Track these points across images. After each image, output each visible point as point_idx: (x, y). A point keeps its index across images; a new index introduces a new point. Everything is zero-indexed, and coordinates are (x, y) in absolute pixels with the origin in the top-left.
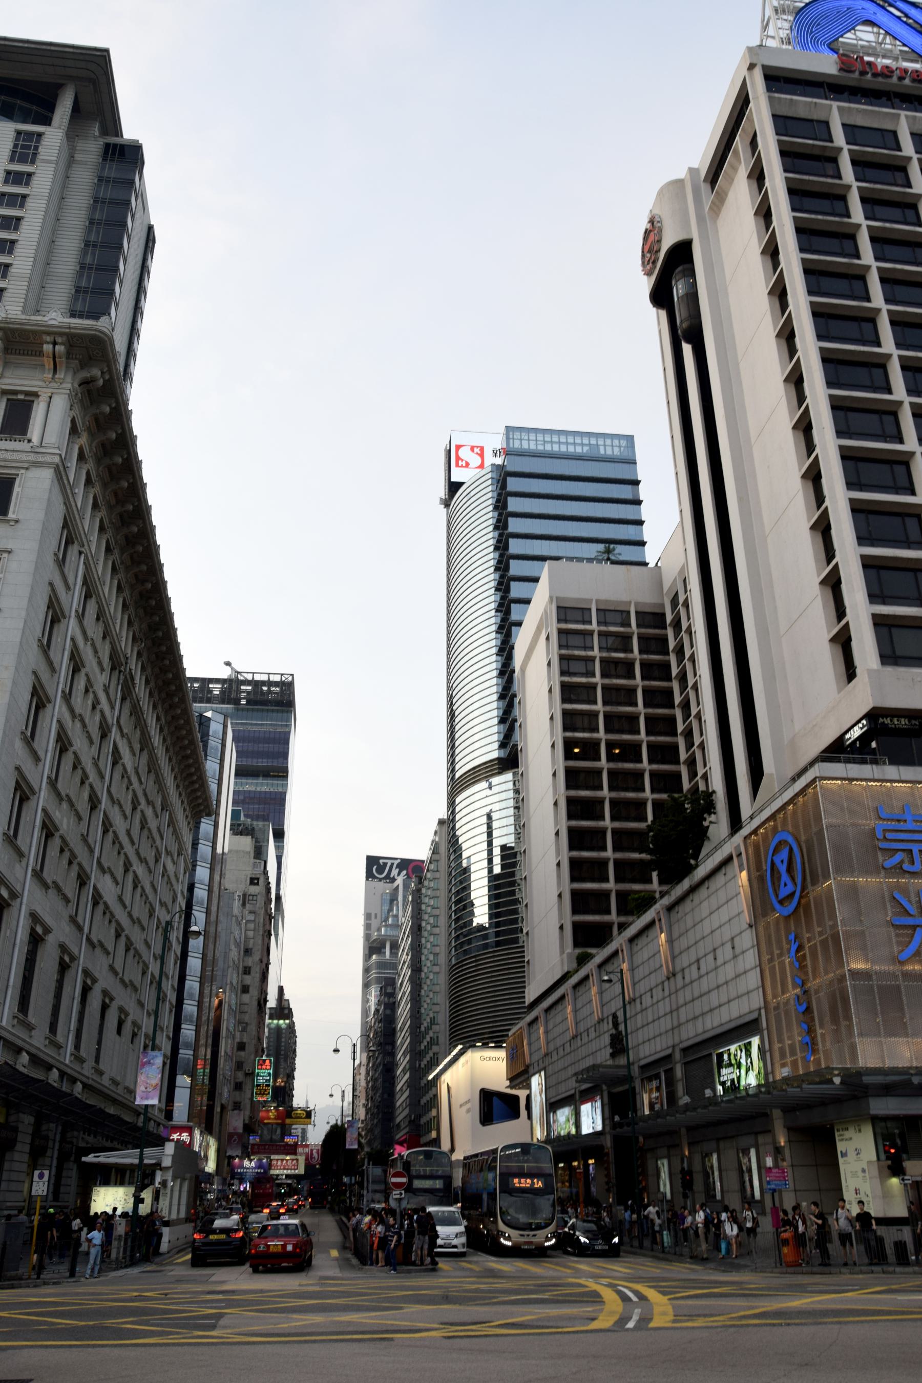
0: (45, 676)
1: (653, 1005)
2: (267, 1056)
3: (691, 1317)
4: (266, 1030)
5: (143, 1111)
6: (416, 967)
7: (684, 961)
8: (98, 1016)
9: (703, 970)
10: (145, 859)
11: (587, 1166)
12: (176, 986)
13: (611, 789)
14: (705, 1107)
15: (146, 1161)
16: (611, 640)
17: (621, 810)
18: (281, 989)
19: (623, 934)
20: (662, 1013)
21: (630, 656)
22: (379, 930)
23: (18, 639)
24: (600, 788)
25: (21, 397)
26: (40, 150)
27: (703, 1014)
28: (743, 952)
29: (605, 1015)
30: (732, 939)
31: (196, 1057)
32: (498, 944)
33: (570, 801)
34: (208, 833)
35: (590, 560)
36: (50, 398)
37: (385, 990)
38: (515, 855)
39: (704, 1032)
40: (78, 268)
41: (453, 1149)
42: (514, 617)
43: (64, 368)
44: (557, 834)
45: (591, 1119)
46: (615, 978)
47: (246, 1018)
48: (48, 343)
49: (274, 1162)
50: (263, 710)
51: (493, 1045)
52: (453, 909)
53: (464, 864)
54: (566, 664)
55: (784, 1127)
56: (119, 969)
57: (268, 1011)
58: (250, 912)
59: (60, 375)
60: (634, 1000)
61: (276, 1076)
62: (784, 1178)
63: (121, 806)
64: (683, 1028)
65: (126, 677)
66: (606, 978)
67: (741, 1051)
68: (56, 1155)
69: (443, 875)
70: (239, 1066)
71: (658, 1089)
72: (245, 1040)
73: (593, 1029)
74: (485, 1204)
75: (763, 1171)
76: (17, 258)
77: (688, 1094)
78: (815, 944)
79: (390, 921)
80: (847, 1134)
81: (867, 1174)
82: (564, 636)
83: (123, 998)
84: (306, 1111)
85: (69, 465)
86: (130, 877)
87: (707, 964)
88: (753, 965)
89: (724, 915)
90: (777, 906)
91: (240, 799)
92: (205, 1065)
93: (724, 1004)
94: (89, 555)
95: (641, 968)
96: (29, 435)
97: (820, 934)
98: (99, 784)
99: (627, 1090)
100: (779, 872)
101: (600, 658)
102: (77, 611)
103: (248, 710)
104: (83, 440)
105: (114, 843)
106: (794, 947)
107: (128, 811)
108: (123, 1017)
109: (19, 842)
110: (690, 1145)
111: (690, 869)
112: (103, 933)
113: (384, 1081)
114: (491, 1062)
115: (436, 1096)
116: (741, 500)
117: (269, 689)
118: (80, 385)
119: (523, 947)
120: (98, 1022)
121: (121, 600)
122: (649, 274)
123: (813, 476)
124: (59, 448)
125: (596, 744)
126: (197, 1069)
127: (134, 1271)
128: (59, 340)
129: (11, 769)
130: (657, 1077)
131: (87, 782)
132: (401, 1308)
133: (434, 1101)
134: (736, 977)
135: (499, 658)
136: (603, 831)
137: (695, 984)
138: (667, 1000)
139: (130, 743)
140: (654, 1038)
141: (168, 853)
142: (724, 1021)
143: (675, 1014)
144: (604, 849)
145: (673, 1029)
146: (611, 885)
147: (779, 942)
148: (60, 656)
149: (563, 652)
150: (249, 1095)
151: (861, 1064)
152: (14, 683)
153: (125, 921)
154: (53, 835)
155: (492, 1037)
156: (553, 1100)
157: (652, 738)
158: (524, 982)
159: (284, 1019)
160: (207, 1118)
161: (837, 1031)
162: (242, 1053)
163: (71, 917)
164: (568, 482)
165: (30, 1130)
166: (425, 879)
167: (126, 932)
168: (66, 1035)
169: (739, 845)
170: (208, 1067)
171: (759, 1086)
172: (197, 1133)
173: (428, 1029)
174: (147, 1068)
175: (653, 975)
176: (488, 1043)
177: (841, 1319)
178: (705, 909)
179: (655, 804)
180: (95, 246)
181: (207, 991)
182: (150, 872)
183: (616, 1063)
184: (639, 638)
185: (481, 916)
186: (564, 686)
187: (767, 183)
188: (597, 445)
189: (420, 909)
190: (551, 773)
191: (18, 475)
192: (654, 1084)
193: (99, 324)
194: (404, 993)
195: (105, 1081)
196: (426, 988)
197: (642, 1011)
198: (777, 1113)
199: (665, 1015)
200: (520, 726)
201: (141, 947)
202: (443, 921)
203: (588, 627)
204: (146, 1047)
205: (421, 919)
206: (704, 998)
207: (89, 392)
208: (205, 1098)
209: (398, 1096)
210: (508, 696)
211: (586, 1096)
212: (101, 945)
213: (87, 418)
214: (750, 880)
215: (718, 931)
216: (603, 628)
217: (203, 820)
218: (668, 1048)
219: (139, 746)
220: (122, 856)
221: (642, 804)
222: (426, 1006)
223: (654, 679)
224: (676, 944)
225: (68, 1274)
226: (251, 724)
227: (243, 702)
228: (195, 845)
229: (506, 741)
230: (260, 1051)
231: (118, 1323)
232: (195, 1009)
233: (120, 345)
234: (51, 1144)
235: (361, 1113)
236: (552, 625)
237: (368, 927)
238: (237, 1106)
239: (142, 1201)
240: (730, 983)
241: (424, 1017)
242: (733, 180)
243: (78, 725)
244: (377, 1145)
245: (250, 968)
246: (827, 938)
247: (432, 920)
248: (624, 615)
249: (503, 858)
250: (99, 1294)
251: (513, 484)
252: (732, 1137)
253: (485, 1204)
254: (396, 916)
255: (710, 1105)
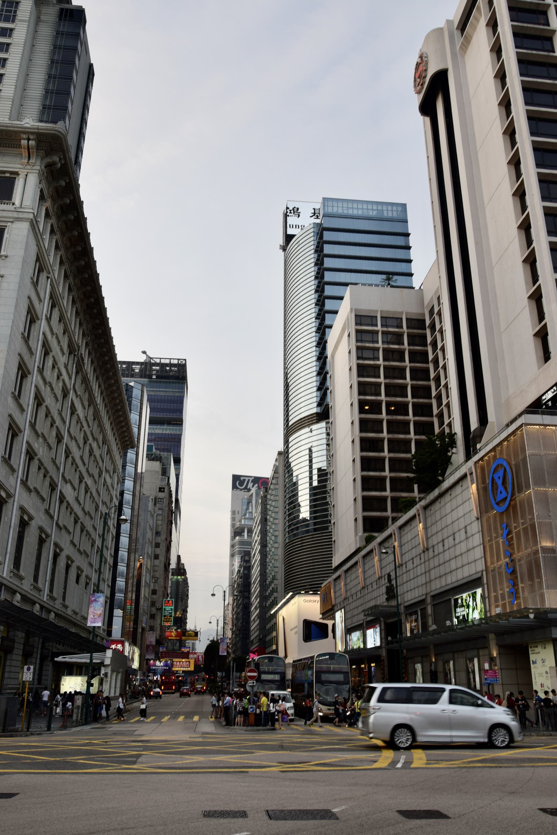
0: (26, 357)
1: (413, 568)
2: (170, 598)
3: (438, 761)
4: (170, 582)
5: (92, 630)
6: (264, 544)
7: (434, 540)
8: (64, 572)
9: (446, 547)
10: (92, 474)
11: (370, 667)
12: (113, 555)
13: (388, 432)
14: (446, 632)
15: (94, 661)
16: (390, 337)
17: (394, 446)
18: (179, 557)
19: (395, 524)
20: (419, 573)
21: (402, 347)
22: (240, 521)
23: (9, 333)
24: (382, 432)
25: (8, 175)
26: (18, 13)
27: (445, 574)
28: (473, 535)
29: (383, 575)
30: (466, 527)
31: (125, 597)
32: (315, 530)
33: (362, 440)
34: (132, 459)
35: (377, 285)
36: (27, 175)
37: (244, 558)
38: (326, 474)
39: (446, 585)
40: (44, 93)
41: (286, 656)
42: (327, 322)
43: (35, 156)
44: (354, 460)
45: (373, 638)
46: (390, 551)
47: (157, 575)
48: (24, 139)
49: (175, 663)
50: (167, 382)
51: (311, 592)
52: (287, 508)
53: (294, 481)
54: (361, 352)
55: (497, 645)
56: (77, 543)
57: (171, 571)
58: (159, 509)
59: (32, 161)
60: (402, 565)
61: (176, 611)
62: (496, 676)
63: (76, 441)
64: (433, 583)
65: (78, 359)
66: (384, 551)
67: (470, 597)
68: (39, 657)
69: (281, 487)
70: (153, 604)
71: (416, 620)
72: (156, 588)
73: (375, 583)
74: (306, 690)
75: (482, 672)
76: (4, 86)
77: (435, 624)
78: (519, 530)
79: (247, 516)
80: (537, 650)
81: (549, 675)
82: (359, 334)
83: (79, 561)
84: (195, 632)
85: (39, 220)
86: (83, 485)
87: (449, 542)
88: (479, 543)
89: (460, 511)
90: (495, 506)
91: (152, 438)
92: (131, 603)
93: (460, 568)
94: (54, 279)
95: (406, 545)
96: (13, 200)
97: (523, 524)
98: (63, 427)
99: (397, 621)
100: (497, 484)
101: (383, 348)
102: (46, 316)
103: (157, 382)
104: (48, 204)
105: (72, 464)
106: (506, 532)
107: (81, 445)
108: (80, 573)
109: (12, 462)
110: (436, 655)
111: (439, 483)
112: (67, 520)
113: (243, 615)
114: (310, 603)
115: (275, 624)
116: (478, 243)
117: (170, 368)
118: (45, 167)
119: (331, 532)
120: (64, 576)
121: (74, 309)
122: (419, 93)
123: (525, 227)
124: (32, 209)
125: (380, 403)
126: (127, 606)
127: (87, 728)
128: (31, 137)
129: (6, 415)
130: (416, 613)
131: (55, 425)
132: (253, 753)
133: (275, 627)
134: (468, 551)
135: (318, 349)
136: (383, 459)
137: (441, 555)
138: (423, 565)
139: (82, 401)
140: (414, 589)
141: (107, 471)
142: (459, 578)
143: (427, 574)
144: (384, 470)
145: (426, 583)
146: (388, 493)
147: (496, 528)
148: (36, 344)
149: (359, 344)
150: (159, 621)
151: (547, 606)
152: (7, 361)
153: (80, 513)
154: (33, 458)
155: (311, 588)
156: (349, 627)
157: (415, 400)
158: (332, 554)
159: (181, 576)
160: (133, 636)
161: (532, 586)
162: (155, 596)
163: (46, 510)
164: (363, 235)
165: (22, 641)
166: (270, 489)
167: (81, 520)
168: (44, 583)
169: (471, 467)
170: (134, 604)
171: (481, 619)
172: (127, 644)
173: (271, 582)
174: (94, 604)
175: (414, 550)
176: (308, 592)
177: (534, 764)
178: (448, 508)
179: (417, 441)
180: (55, 78)
181: (132, 558)
182: (96, 483)
183: (390, 604)
184: (408, 336)
185: (305, 513)
186: (359, 366)
187: (499, 29)
188: (383, 210)
189: (266, 508)
190: (350, 422)
191: (6, 226)
192: (414, 617)
193: (57, 126)
194: (256, 560)
195: (69, 612)
196: (269, 557)
197: (406, 572)
198: (492, 636)
199: (421, 575)
200: (331, 392)
201: (90, 529)
202: (280, 515)
203: (375, 328)
204: (94, 592)
205: (267, 514)
206: (447, 564)
207: (52, 172)
208: (132, 624)
209: (252, 624)
210: (323, 373)
211: (370, 625)
212: (66, 528)
213: (50, 189)
214: (478, 489)
215: (457, 522)
216: (385, 329)
217: (129, 451)
218: (423, 595)
219: (87, 403)
220: (78, 472)
221: (409, 441)
222: (269, 568)
223: (418, 362)
224: (429, 530)
225: (46, 729)
226: (159, 391)
227: (154, 377)
228: (124, 467)
229: (322, 402)
230: (166, 595)
231: (75, 759)
232: (125, 568)
233: (72, 141)
234: (35, 650)
235: (229, 634)
236: (352, 326)
237: (233, 519)
238: (152, 628)
239: (92, 685)
240: (463, 555)
241: (268, 575)
242: (476, 28)
243: (48, 389)
244: (239, 653)
245: (159, 544)
246: (527, 527)
247: (273, 515)
248: (399, 320)
249: (319, 476)
250: (64, 741)
251: (327, 236)
252: (463, 651)
253: (306, 690)
254: (251, 513)
255: (450, 630)
